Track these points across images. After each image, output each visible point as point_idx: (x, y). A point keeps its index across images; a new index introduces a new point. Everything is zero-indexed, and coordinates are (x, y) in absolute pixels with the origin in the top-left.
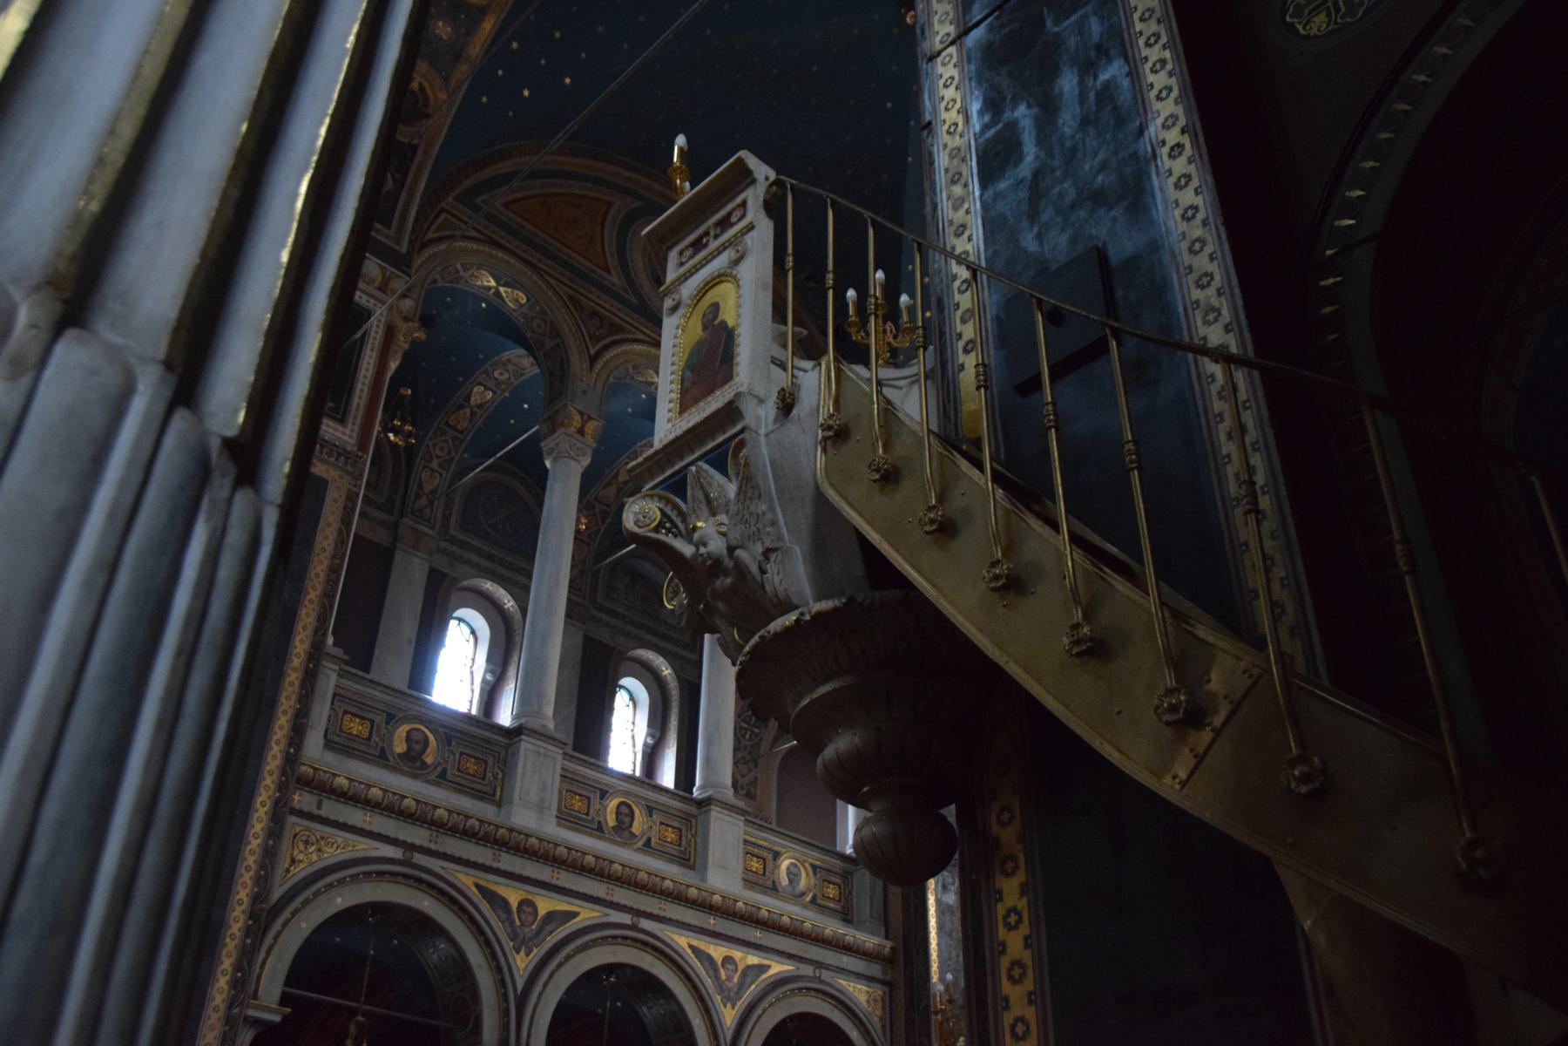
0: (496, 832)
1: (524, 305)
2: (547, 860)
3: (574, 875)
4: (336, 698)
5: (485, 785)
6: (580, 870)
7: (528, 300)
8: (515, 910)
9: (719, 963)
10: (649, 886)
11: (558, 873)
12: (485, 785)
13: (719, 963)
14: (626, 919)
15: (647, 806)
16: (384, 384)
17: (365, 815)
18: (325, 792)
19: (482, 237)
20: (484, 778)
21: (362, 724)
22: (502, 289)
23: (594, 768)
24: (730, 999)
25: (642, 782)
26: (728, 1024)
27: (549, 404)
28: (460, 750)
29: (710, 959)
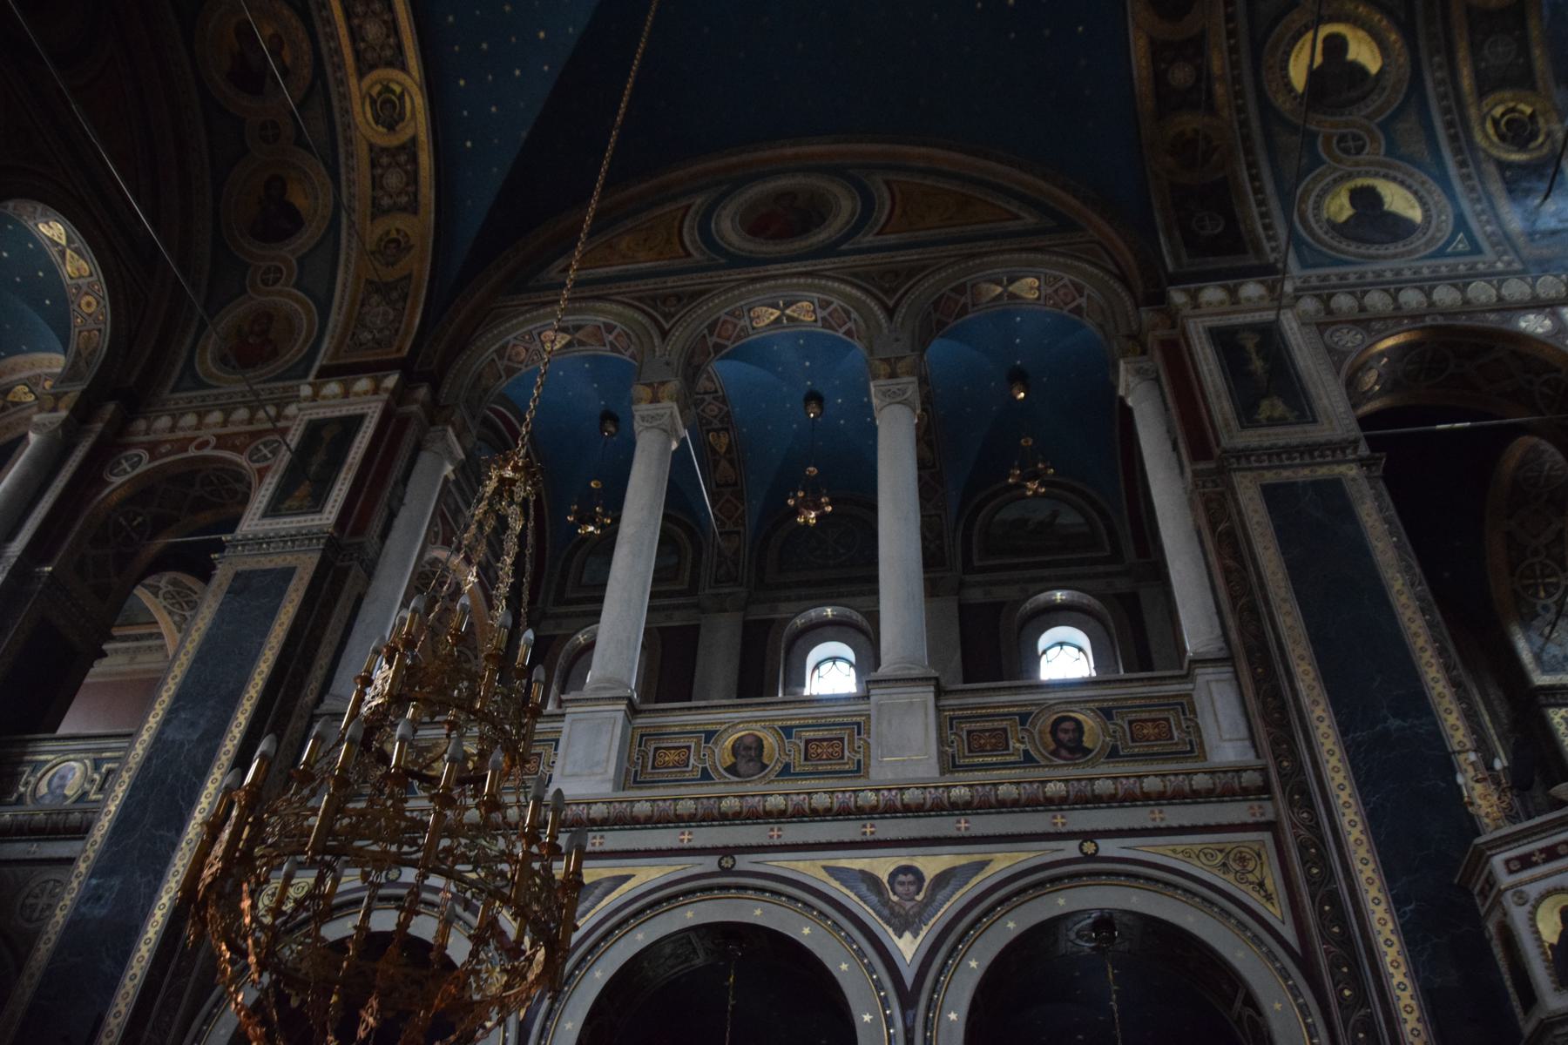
0: (1141, 784)
1: (1039, 286)
2: (1234, 795)
3: (908, 820)
4: (954, 722)
5: (844, 764)
6: (1132, 801)
7: (1039, 279)
8: (887, 885)
9: (885, 880)
10: (1072, 797)
11: (1161, 812)
12: (1176, 744)
13: (885, 880)
14: (1071, 849)
15: (1101, 709)
16: (29, 457)
17: (1153, 812)
18: (1041, 806)
19: (952, 260)
20: (842, 758)
21: (1158, 725)
22: (999, 290)
23: (1045, 690)
24: (904, 924)
25: (1104, 682)
26: (908, 958)
27: (62, 382)
28: (1126, 719)
29: (871, 880)
